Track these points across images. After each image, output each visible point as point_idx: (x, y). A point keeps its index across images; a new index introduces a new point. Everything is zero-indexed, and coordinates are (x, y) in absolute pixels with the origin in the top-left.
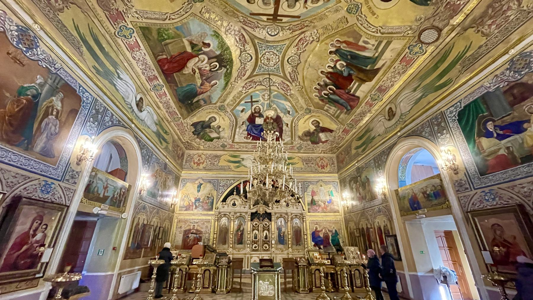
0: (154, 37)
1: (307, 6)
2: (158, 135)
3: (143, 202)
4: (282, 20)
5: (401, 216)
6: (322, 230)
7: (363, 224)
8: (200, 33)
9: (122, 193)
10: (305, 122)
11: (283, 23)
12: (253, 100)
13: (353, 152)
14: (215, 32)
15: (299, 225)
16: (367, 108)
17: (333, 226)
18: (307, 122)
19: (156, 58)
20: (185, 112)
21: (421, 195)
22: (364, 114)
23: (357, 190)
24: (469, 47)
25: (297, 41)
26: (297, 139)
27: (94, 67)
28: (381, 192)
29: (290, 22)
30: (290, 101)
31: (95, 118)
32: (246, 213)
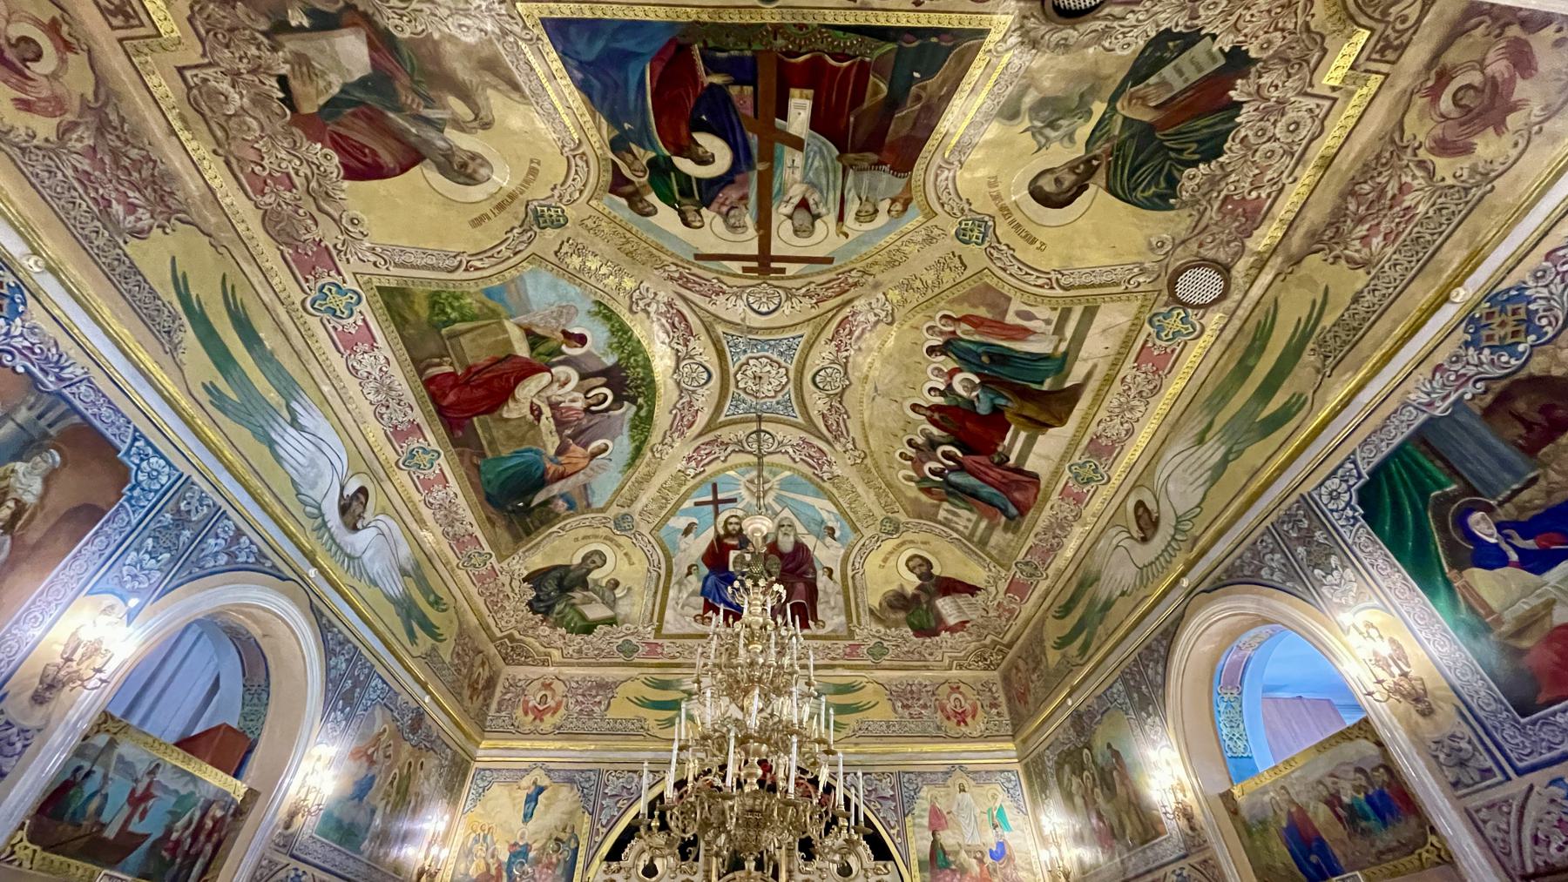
0: (417, 314)
1: (845, 229)
2: (406, 609)
3: (294, 863)
4: (783, 271)
9: (209, 824)
11: (789, 278)
12: (720, 496)
13: (1053, 657)
16: (1067, 509)
19: (421, 373)
20: (505, 537)
23: (1089, 802)
24: (1324, 303)
26: (865, 618)
27: (211, 389)
28: (1171, 805)
29: (806, 276)
30: (831, 498)
31: (165, 538)
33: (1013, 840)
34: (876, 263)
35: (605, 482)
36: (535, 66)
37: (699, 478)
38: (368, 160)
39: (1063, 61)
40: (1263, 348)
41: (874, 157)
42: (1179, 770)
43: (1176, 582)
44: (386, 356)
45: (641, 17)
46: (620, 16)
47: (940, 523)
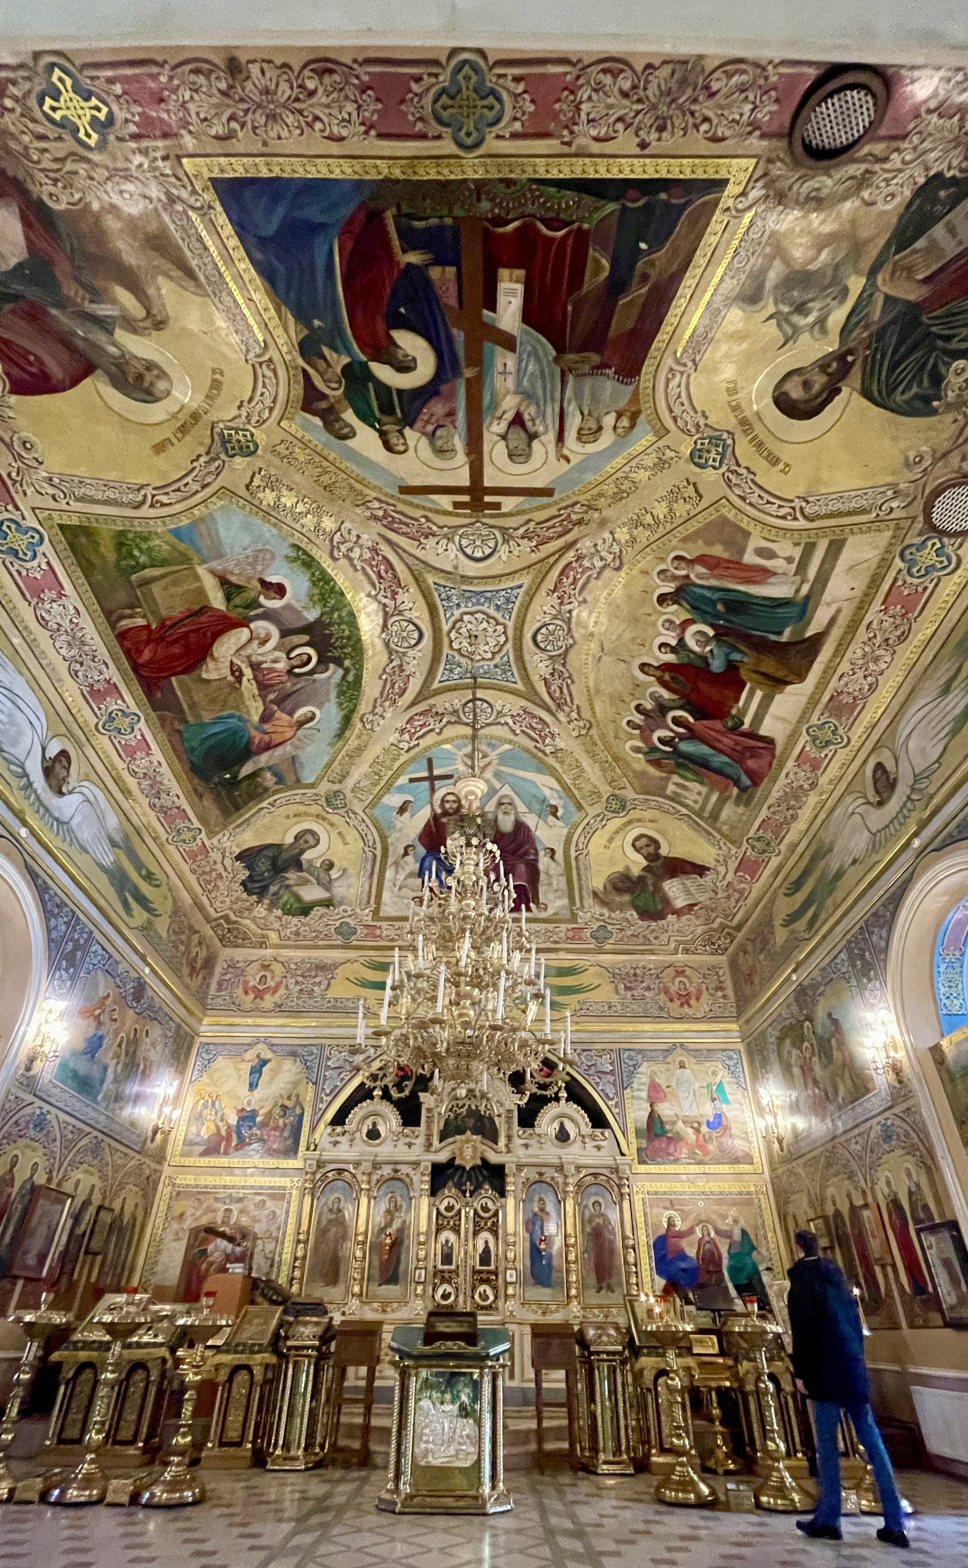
0: (103, 557)
1: (566, 452)
2: (119, 880)
3: (39, 1103)
4: (497, 506)
6: (691, 1231)
7: (838, 1195)
8: (249, 552)
10: (611, 840)
11: (504, 515)
12: (436, 772)
13: (781, 935)
14: (299, 548)
18: (617, 842)
19: (113, 625)
20: (214, 812)
22: (797, 798)
25: (555, 573)
26: (589, 901)
28: (881, 1060)
29: (524, 512)
30: (553, 773)
32: (416, 1164)
33: (730, 1112)
34: (601, 495)
35: (314, 753)
36: (209, 243)
37: (413, 752)
38: (33, 370)
39: (822, 223)
41: (596, 358)
42: (894, 1029)
43: (908, 844)
44: (74, 606)
45: (324, 173)
46: (301, 173)
47: (668, 798)
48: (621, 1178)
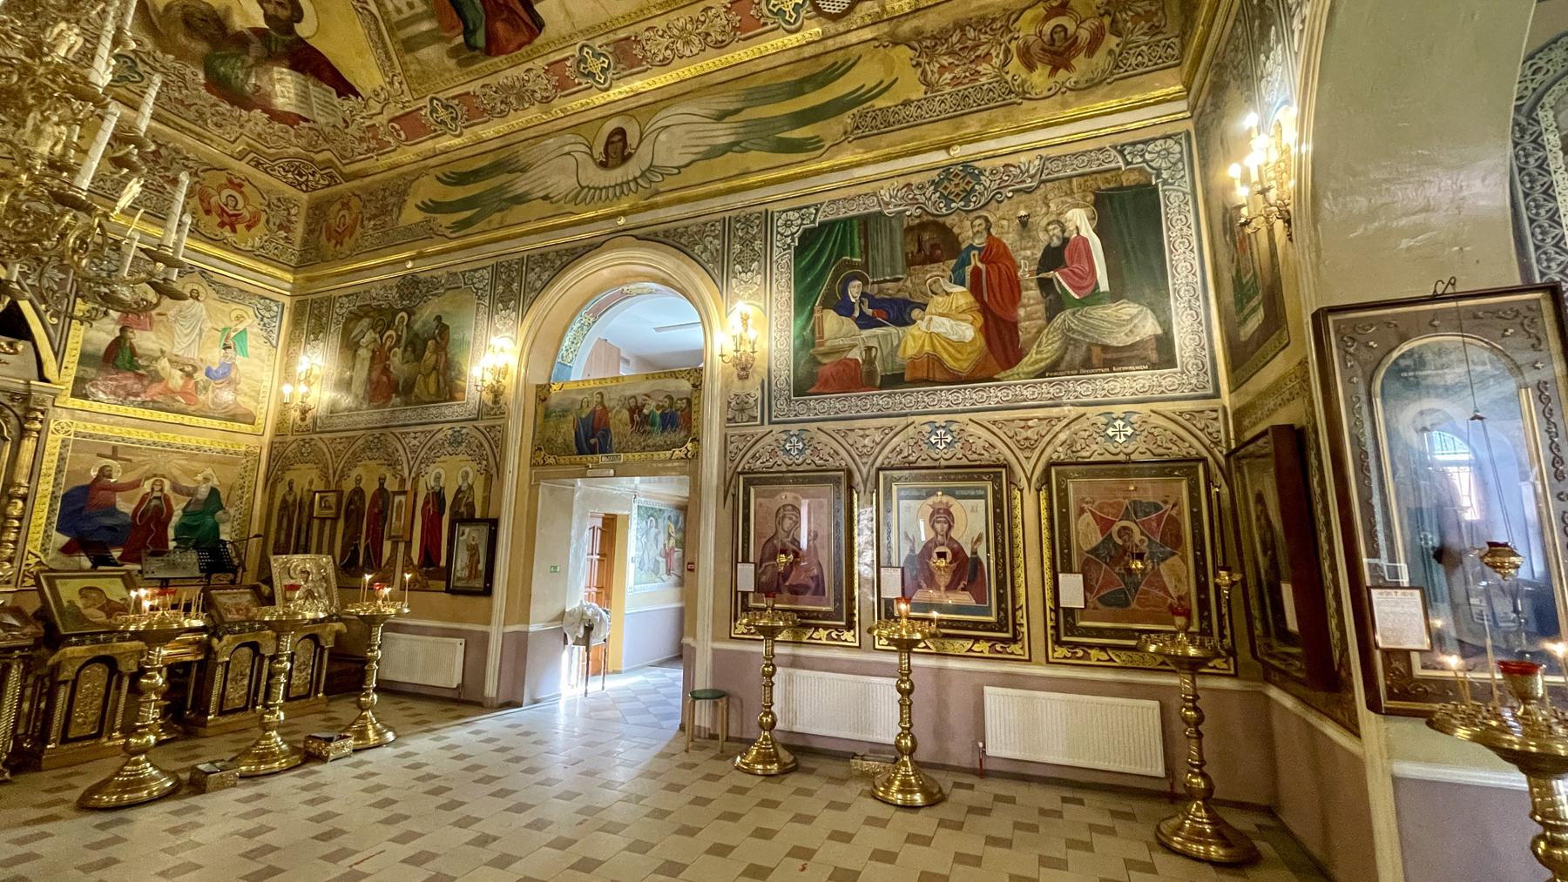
5: (533, 466)
6: (136, 485)
7: (366, 475)
13: (411, 215)
15: (1032, 356)
16: (541, 85)
17: (209, 471)
21: (625, 414)
40: (823, 85)
48: (29, 410)
